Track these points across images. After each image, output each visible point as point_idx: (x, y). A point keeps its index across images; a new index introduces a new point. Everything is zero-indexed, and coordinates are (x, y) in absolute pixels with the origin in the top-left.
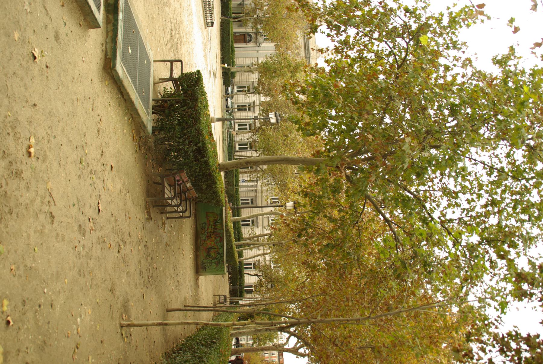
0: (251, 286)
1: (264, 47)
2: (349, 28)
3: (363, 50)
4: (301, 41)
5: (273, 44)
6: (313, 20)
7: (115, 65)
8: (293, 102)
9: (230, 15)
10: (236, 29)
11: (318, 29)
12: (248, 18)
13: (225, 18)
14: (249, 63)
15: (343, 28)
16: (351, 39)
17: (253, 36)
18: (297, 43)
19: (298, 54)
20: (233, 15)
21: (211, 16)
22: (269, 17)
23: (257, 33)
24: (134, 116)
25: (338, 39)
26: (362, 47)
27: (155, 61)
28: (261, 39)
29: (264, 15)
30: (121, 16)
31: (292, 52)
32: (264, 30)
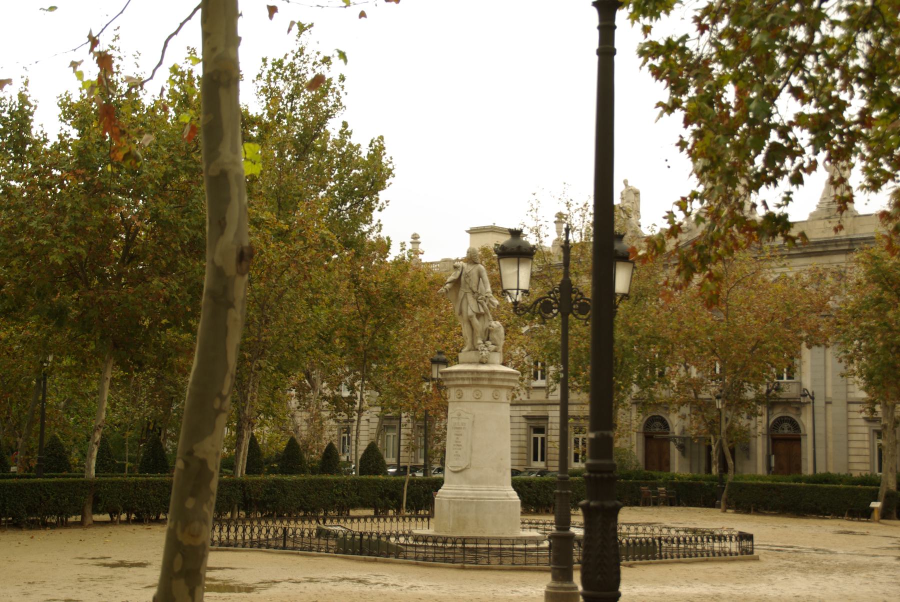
1: (814, 380)
2: (775, 119)
3: (845, 71)
4: (798, 268)
5: (807, 354)
6: (747, 226)
9: (714, 479)
10: (758, 465)
11: (777, 212)
12: (724, 427)
13: (724, 495)
14: (524, 426)
15: (774, 136)
16: (810, 109)
18: (806, 277)
19: (840, 276)
20: (715, 470)
21: (721, 538)
22: (722, 362)
23: (771, 401)
25: (809, 150)
26: (837, 74)
28: (790, 391)
29: (714, 377)
31: (834, 292)
32: (761, 380)
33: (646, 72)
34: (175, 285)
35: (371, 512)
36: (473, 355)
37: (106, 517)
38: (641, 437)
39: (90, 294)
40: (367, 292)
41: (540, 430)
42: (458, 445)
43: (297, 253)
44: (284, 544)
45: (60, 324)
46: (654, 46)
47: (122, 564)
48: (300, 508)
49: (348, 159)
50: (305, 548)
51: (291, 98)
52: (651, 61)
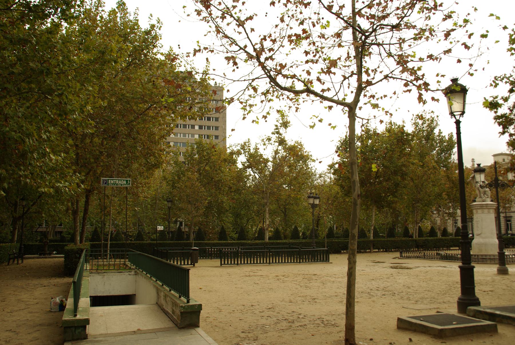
30: (498, 312)
34: (390, 184)
35: (458, 248)
36: (480, 199)
37: (377, 250)
40: (452, 180)
42: (478, 227)
43: (426, 171)
44: (424, 257)
46: (498, 116)
47: (378, 262)
48: (434, 247)
49: (442, 141)
50: (431, 258)
51: (422, 124)
52: (498, 121)
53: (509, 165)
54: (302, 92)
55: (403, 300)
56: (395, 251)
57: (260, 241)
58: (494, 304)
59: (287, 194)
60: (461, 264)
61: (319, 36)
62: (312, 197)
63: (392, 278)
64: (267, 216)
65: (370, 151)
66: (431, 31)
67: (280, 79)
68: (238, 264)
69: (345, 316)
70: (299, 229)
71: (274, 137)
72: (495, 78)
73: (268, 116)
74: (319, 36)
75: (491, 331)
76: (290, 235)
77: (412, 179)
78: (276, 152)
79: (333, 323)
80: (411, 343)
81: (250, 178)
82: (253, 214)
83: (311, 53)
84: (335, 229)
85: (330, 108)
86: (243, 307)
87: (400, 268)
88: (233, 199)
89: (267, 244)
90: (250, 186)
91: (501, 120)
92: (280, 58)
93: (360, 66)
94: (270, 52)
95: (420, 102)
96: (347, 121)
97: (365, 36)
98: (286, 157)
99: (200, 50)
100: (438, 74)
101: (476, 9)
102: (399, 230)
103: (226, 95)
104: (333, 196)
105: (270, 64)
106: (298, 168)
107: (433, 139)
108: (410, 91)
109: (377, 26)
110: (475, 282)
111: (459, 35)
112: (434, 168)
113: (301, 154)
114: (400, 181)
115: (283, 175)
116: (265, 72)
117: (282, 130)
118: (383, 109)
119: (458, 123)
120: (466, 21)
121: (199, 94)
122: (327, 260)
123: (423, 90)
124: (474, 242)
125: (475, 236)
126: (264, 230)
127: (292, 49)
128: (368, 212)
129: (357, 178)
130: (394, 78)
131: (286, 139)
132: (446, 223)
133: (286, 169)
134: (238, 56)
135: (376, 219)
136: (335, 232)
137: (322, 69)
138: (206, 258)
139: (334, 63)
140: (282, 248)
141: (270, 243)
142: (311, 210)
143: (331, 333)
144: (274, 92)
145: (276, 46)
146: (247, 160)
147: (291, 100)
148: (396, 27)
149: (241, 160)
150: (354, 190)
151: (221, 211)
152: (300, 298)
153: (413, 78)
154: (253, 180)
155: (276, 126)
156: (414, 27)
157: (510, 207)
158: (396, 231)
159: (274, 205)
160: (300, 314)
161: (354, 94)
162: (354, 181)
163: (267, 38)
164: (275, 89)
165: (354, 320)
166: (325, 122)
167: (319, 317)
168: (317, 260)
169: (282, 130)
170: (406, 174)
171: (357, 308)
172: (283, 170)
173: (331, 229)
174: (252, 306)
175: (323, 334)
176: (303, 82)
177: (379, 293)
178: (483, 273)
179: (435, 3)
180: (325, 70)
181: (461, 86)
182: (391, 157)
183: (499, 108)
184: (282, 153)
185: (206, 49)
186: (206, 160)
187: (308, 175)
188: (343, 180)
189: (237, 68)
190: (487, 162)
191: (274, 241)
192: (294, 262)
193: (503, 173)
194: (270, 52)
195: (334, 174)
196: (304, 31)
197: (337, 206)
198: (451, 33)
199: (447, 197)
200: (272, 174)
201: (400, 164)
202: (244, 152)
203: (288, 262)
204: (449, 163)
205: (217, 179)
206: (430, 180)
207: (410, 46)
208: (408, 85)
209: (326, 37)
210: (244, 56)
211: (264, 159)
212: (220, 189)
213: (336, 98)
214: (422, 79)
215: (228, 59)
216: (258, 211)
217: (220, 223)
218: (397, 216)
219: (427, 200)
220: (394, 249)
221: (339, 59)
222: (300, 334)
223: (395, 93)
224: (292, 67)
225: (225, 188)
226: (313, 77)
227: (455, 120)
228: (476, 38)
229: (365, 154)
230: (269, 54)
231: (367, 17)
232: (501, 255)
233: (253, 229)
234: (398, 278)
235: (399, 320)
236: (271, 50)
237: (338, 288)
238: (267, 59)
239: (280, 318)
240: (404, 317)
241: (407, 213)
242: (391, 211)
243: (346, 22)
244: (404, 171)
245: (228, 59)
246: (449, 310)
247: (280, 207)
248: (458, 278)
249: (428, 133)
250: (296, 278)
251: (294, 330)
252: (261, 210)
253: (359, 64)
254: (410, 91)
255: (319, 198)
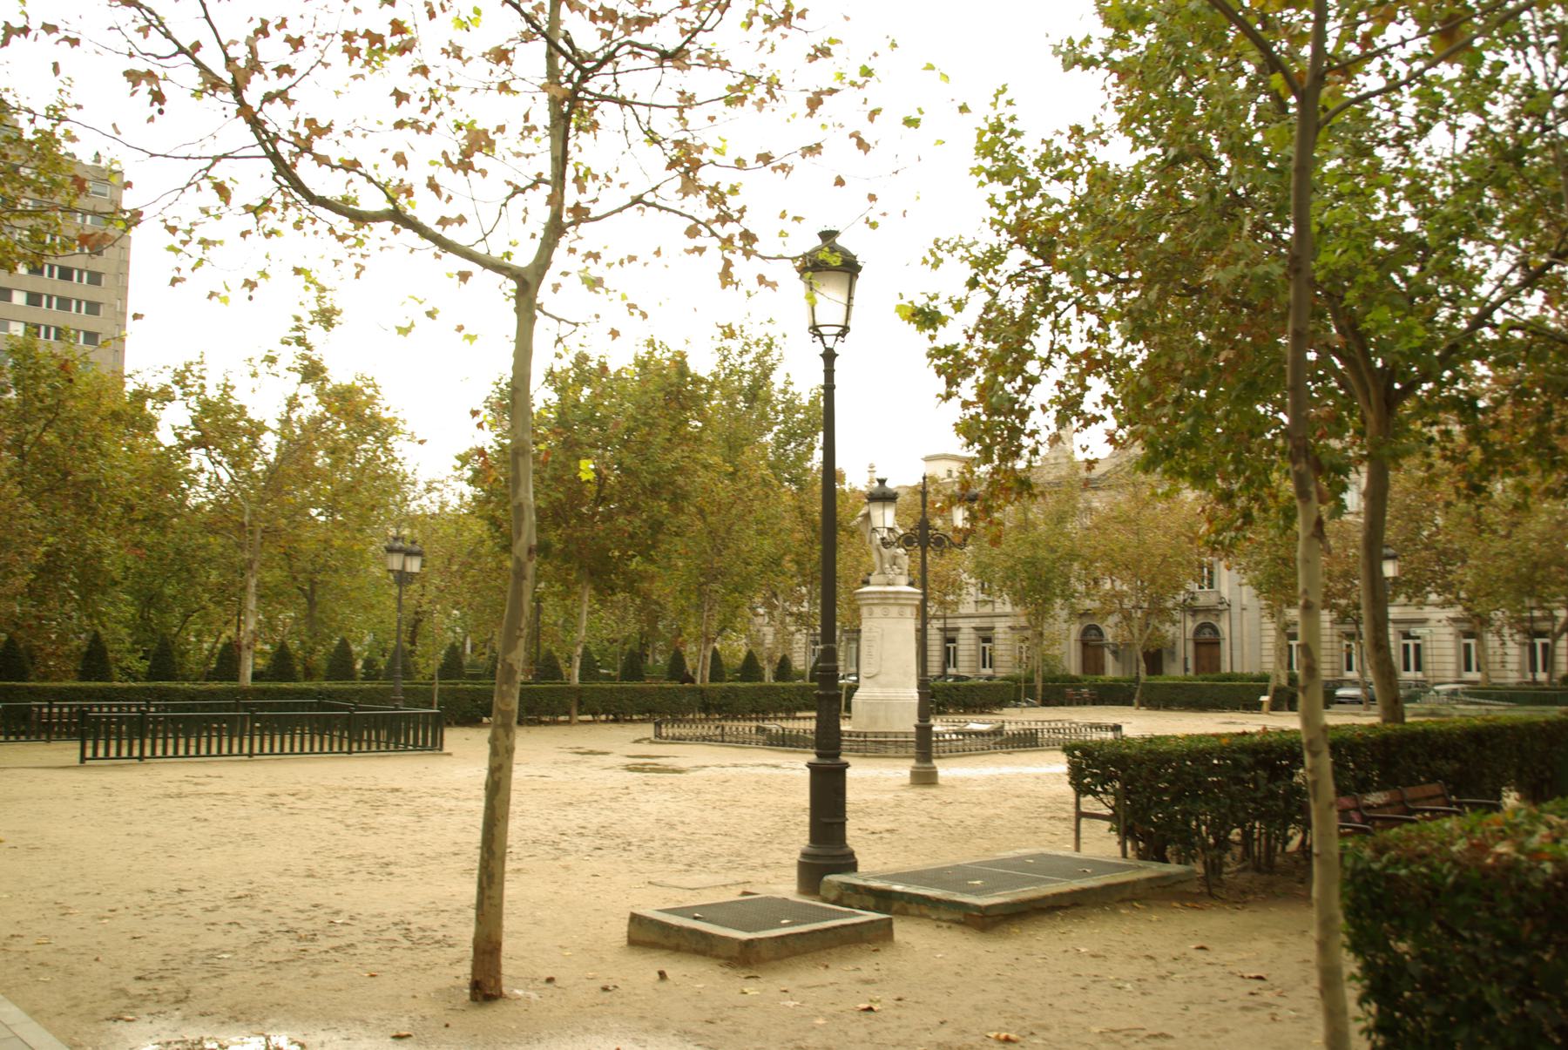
0: (1533, 648)
1: (1230, 589)
7: (977, 908)
8: (1244, 524)
17: (1201, 619)
24: (1127, 894)
27: (1078, 849)
30: (898, 888)
33: (933, 370)
34: (637, 522)
36: (881, 578)
37: (589, 717)
38: (1079, 644)
39: (569, 531)
41: (987, 640)
44: (722, 740)
45: (546, 557)
46: (937, 350)
47: (591, 753)
48: (752, 711)
49: (790, 407)
50: (741, 742)
51: (741, 354)
52: (936, 361)
53: (956, 488)
54: (377, 217)
55: (653, 861)
56: (642, 721)
57: (224, 685)
58: (897, 864)
59: (321, 537)
60: (813, 758)
61: (444, 51)
62: (400, 551)
63: (625, 798)
64: (252, 603)
65: (585, 422)
66: (772, 85)
67: (306, 170)
68: (141, 757)
69: (472, 913)
70: (355, 648)
71: (290, 356)
72: (936, 242)
73: (261, 282)
74: (444, 51)
75: (877, 936)
76: (324, 666)
77: (701, 511)
78: (293, 403)
79: (439, 936)
80: (662, 986)
81: (203, 478)
82: (207, 596)
83: (414, 99)
84: (468, 651)
85: (464, 276)
86: (147, 898)
87: (652, 770)
88: (138, 545)
89: (245, 692)
90: (198, 508)
91: (944, 360)
92: (312, 100)
93: (561, 160)
94: (280, 76)
95: (724, 286)
96: (509, 321)
97: (583, 70)
98: (323, 419)
99: (25, 30)
100: (785, 213)
101: (894, 45)
102: (658, 659)
103: (129, 201)
104: (465, 551)
105: (277, 117)
106: (361, 458)
107: (767, 401)
108: (701, 250)
109: (620, 46)
110: (849, 807)
111: (844, 109)
112: (765, 482)
113: (372, 416)
114: (667, 516)
115: (307, 475)
116: (259, 138)
117: (315, 334)
118: (624, 297)
119: (829, 356)
120: (867, 73)
121: (27, 182)
122: (436, 746)
123: (740, 252)
124: (859, 695)
125: (862, 680)
126: (239, 647)
127: (355, 77)
128: (568, 602)
129: (528, 496)
130: (661, 208)
131: (325, 364)
132: (790, 642)
133: (321, 460)
134: (170, 73)
135: (589, 626)
136: (467, 661)
137: (445, 154)
138: (28, 740)
139: (479, 141)
140: (295, 707)
141: (257, 690)
142: (395, 591)
143: (430, 966)
144: (286, 206)
145: (300, 62)
146: (194, 422)
147: (342, 238)
148: (675, 57)
149: (173, 421)
150: (519, 533)
151: (92, 582)
152: (341, 864)
153: (713, 213)
154: (209, 488)
155: (298, 319)
156: (724, 65)
157: (957, 604)
158: (650, 662)
159: (277, 572)
160: (337, 913)
161: (537, 243)
162: (521, 505)
163: (271, 28)
164: (289, 200)
165: (499, 926)
166: (446, 321)
167: (397, 919)
168: (407, 743)
169: (315, 334)
170: (685, 497)
171: (512, 889)
172: (313, 461)
173: (454, 653)
174: (180, 891)
175: (406, 970)
176: (383, 188)
177: (585, 844)
178: (872, 782)
179: (789, 6)
180: (455, 159)
181: (845, 252)
182: (645, 443)
183: (940, 327)
184: (311, 407)
185: (50, 28)
186: (49, 409)
187: (392, 484)
188: (498, 504)
189: (161, 112)
190: (904, 476)
191: (272, 685)
192: (331, 751)
193: (941, 509)
194: (280, 76)
195: (471, 482)
196: (398, 27)
197: (476, 582)
198: (825, 98)
199: (794, 568)
200: (273, 471)
201: (669, 465)
202: (185, 394)
203: (312, 751)
204: (806, 470)
205: (82, 476)
206: (750, 518)
207: (712, 119)
208: (698, 233)
209: (465, 55)
210: (194, 78)
211: (249, 421)
212: (93, 511)
213: (480, 249)
214: (738, 221)
215: (133, 77)
216: (222, 588)
217: (86, 622)
218: (654, 619)
219: (738, 575)
220: (638, 713)
221: (501, 129)
222: (332, 975)
223: (658, 253)
224: (348, 133)
225: (109, 508)
226: (415, 176)
227: (822, 350)
228: (890, 122)
229: (570, 429)
230: (275, 84)
231: (593, 13)
232: (924, 731)
233: (201, 646)
234: (644, 797)
235: (635, 919)
236: (283, 70)
237: (463, 830)
238: (269, 98)
239: (272, 925)
240: (649, 912)
241: (682, 611)
242: (638, 601)
243: (528, 18)
244: (680, 487)
245: (133, 77)
246: (774, 887)
247: (295, 579)
248: (802, 797)
249: (755, 380)
250: (334, 802)
251: (313, 962)
252: (233, 583)
253: (559, 154)
254: (701, 250)
255: (419, 554)
